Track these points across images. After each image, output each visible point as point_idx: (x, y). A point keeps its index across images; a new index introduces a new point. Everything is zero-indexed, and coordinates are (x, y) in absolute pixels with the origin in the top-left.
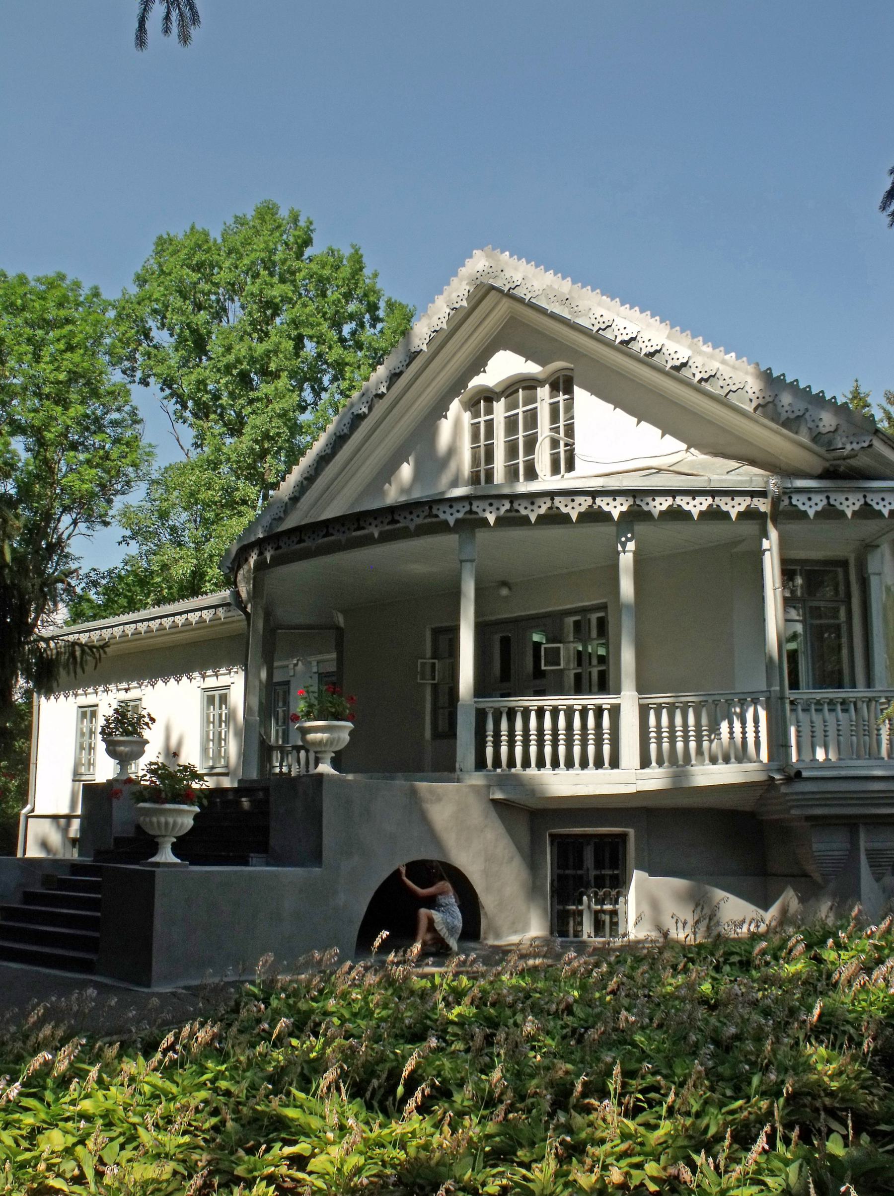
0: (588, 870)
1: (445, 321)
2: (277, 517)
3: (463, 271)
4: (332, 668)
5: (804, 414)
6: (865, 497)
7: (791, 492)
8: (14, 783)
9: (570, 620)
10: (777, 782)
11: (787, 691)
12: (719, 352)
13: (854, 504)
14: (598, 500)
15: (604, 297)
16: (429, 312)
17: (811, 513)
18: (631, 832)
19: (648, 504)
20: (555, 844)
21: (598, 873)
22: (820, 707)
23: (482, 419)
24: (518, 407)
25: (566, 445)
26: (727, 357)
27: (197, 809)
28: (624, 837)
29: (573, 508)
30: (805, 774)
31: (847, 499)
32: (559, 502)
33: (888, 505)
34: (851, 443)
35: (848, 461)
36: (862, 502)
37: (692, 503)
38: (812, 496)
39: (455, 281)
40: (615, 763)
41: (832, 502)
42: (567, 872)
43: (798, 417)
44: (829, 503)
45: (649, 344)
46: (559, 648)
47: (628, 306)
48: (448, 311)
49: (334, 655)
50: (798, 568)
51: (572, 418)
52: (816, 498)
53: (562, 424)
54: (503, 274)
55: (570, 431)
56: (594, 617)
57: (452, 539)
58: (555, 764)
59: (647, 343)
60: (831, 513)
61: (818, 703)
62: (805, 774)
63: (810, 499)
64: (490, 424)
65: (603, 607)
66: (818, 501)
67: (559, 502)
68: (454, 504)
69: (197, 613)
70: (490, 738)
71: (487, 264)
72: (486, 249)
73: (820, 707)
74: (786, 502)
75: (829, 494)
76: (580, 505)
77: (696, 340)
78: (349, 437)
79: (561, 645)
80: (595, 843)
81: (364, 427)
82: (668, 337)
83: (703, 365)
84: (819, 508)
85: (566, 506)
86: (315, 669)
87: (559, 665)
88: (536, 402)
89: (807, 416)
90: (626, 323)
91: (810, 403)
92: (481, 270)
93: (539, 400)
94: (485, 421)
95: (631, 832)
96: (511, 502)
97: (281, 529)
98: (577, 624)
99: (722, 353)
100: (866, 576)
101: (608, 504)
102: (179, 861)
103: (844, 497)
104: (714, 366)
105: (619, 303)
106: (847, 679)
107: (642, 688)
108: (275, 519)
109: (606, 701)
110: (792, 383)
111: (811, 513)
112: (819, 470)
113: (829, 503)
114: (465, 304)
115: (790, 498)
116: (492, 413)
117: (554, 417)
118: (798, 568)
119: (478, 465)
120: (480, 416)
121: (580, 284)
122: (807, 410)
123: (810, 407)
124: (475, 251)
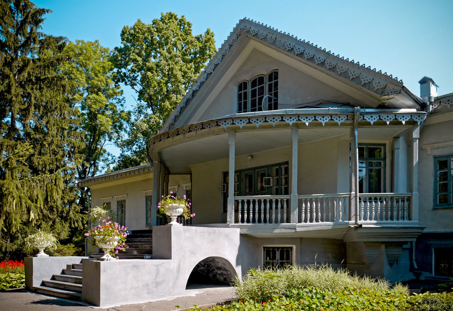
0: (278, 260)
4: (189, 189)
6: (380, 116)
7: (364, 114)
11: (358, 194)
13: (374, 119)
17: (372, 123)
18: (294, 247)
20: (265, 251)
21: (281, 261)
23: (243, 92)
25: (275, 100)
28: (291, 248)
30: (363, 226)
31: (388, 117)
35: (389, 100)
36: (394, 118)
38: (373, 115)
41: (381, 118)
42: (284, 261)
43: (369, 82)
44: (380, 119)
45: (308, 55)
46: (270, 179)
50: (365, 147)
51: (277, 89)
52: (374, 116)
53: (273, 92)
55: (276, 95)
56: (283, 167)
59: (308, 55)
60: (381, 123)
61: (370, 199)
62: (363, 226)
64: (245, 94)
65: (287, 163)
66: (261, 120)
70: (246, 211)
74: (362, 118)
75: (380, 115)
76: (406, 118)
79: (271, 178)
84: (376, 120)
87: (270, 185)
88: (263, 84)
90: (300, 47)
101: (337, 119)
106: (367, 149)
107: (299, 193)
110: (368, 68)
111: (372, 123)
112: (377, 106)
113: (380, 119)
115: (364, 116)
116: (246, 89)
117: (270, 90)
118: (365, 147)
120: (242, 91)
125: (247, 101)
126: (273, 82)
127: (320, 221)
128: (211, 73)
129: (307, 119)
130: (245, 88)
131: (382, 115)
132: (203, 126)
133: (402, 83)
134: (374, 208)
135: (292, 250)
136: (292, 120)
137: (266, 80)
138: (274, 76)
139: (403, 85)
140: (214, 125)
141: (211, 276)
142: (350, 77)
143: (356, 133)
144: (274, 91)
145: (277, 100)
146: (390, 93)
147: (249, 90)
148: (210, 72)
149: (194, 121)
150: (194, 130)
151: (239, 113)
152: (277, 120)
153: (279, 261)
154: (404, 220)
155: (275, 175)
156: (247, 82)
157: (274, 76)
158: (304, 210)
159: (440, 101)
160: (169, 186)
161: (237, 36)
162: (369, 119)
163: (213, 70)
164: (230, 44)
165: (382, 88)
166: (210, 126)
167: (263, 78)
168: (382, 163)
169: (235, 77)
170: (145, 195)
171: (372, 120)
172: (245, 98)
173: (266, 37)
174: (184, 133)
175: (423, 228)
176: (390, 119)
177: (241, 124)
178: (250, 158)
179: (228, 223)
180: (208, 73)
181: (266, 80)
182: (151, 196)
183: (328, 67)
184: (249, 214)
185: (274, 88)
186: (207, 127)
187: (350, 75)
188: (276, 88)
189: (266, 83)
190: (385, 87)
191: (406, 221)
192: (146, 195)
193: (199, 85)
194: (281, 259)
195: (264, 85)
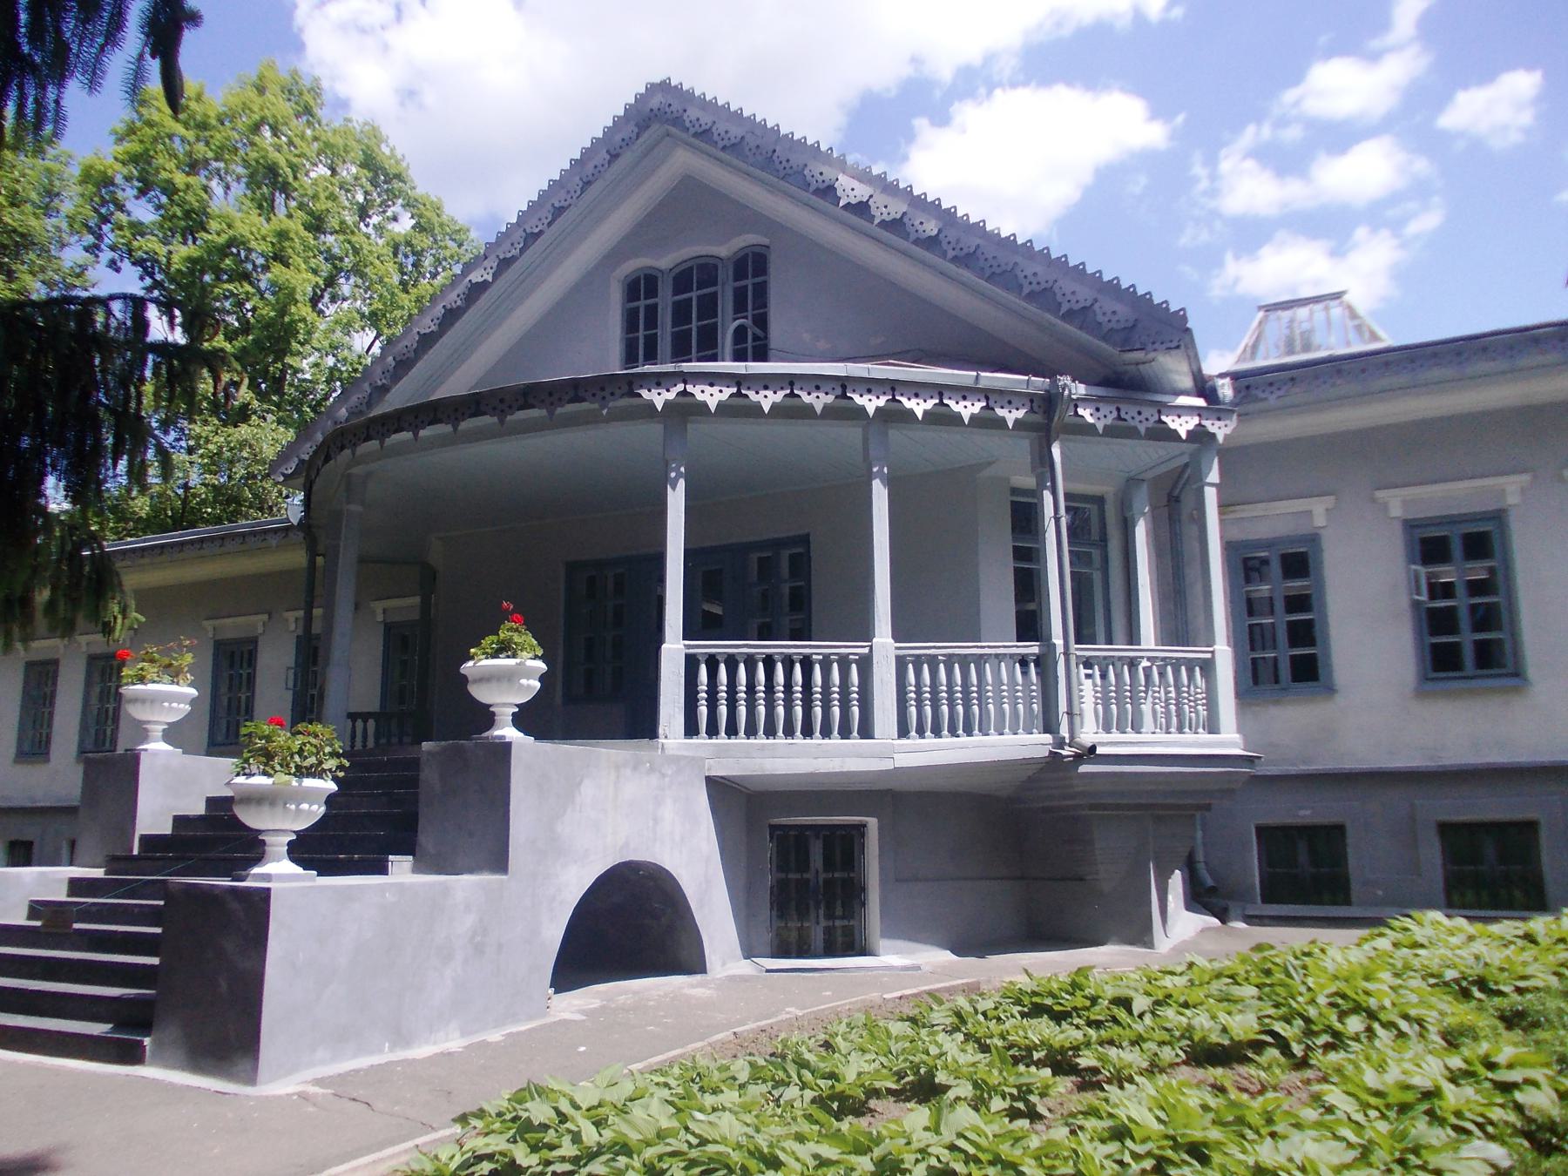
2: (355, 410)
5: (1092, 305)
8: (47, 711)
9: (754, 556)
13: (1147, 419)
18: (872, 823)
22: (1090, 672)
23: (642, 304)
25: (756, 338)
27: (332, 786)
28: (861, 828)
30: (1099, 751)
33: (1184, 424)
40: (866, 732)
41: (1123, 415)
43: (1084, 308)
51: (765, 306)
57: (655, 430)
58: (789, 732)
62: (1099, 751)
64: (652, 311)
66: (1107, 413)
73: (1090, 672)
78: (465, 312)
80: (825, 836)
81: (484, 300)
83: (958, 241)
85: (809, 394)
89: (1096, 306)
91: (1099, 291)
95: (872, 823)
97: (377, 411)
98: (793, 559)
100: (1128, 515)
108: (353, 413)
109: (855, 649)
113: (1119, 418)
117: (740, 307)
122: (1096, 300)
126: (749, 282)
127: (992, 731)
128: (541, 232)
130: (652, 291)
133: (1184, 319)
134: (990, 694)
135: (863, 835)
137: (726, 276)
138: (753, 264)
139: (1188, 325)
140: (618, 392)
142: (1021, 287)
143: (1056, 451)
144: (753, 310)
145: (766, 338)
146: (1150, 347)
147: (666, 300)
148: (536, 230)
149: (457, 385)
150: (494, 409)
151: (626, 369)
153: (822, 876)
157: (753, 264)
158: (743, 695)
160: (315, 604)
161: (636, 130)
164: (613, 152)
165: (1125, 328)
166: (603, 394)
167: (715, 267)
168: (1096, 554)
169: (614, 256)
170: (210, 635)
172: (652, 321)
173: (740, 142)
174: (502, 411)
176: (1147, 419)
179: (661, 740)
180: (528, 231)
181: (726, 276)
183: (951, 254)
184: (716, 707)
185: (754, 303)
186: (594, 395)
187: (1025, 283)
189: (723, 284)
190: (1134, 326)
191: (1203, 736)
192: (217, 638)
194: (826, 870)
195: (719, 288)
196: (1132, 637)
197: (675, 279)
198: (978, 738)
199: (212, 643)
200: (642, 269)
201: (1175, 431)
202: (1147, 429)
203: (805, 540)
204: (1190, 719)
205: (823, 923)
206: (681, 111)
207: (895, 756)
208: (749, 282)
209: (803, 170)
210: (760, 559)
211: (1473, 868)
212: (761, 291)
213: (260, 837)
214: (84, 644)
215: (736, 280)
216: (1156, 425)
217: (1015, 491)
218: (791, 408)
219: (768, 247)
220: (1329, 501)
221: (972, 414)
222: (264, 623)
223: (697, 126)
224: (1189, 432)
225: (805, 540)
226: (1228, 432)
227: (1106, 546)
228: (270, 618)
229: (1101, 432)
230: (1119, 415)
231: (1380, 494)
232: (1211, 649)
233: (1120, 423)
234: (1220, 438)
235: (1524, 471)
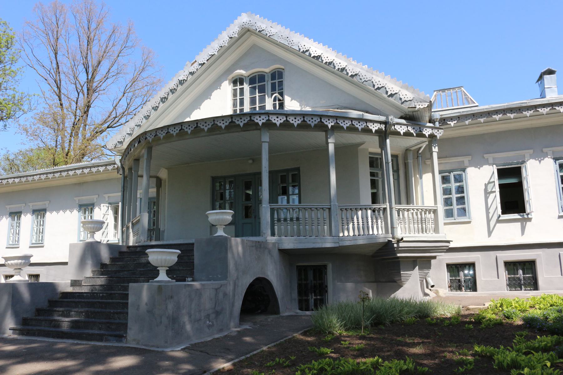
1: (226, 42)
3: (236, 22)
6: (420, 128)
10: (393, 242)
12: (360, 65)
13: (347, 124)
14: (271, 116)
15: (306, 38)
16: (218, 38)
19: (326, 122)
24: (256, 83)
26: (364, 67)
29: (312, 122)
30: (404, 239)
32: (355, 123)
33: (346, 124)
34: (419, 105)
36: (302, 119)
37: (373, 126)
39: (232, 26)
47: (317, 42)
48: (228, 38)
49: (120, 194)
51: (282, 89)
54: (256, 24)
62: (404, 239)
63: (344, 121)
66: (299, 119)
67: (355, 123)
68: (261, 116)
69: (6, 180)
71: (248, 19)
72: (247, 13)
77: (349, 59)
82: (336, 57)
83: (353, 69)
86: (31, 208)
88: (265, 81)
92: (245, 22)
93: (266, 80)
94: (240, 89)
96: (286, 117)
99: (362, 65)
101: (292, 120)
102: (170, 280)
103: (328, 119)
104: (357, 70)
105: (313, 41)
114: (236, 36)
119: (236, 107)
120: (237, 86)
121: (294, 32)
123: (400, 89)
124: (242, 14)
125: (243, 98)
128: (204, 63)
129: (241, 120)
131: (409, 127)
132: (232, 120)
135: (326, 269)
136: (361, 125)
137: (268, 78)
141: (277, 358)
145: (283, 100)
148: (202, 63)
152: (315, 121)
154: (419, 233)
155: (291, 182)
156: (244, 78)
159: (277, 116)
162: (326, 122)
163: (207, 60)
167: (264, 76)
171: (223, 124)
175: (448, 242)
177: (278, 121)
178: (250, 161)
181: (268, 78)
182: (534, 285)
188: (281, 88)
189: (267, 81)
193: (187, 75)
195: (266, 83)
196: (400, 202)
197: (250, 79)
198: (425, 234)
199: (78, 205)
200: (238, 75)
201: (425, 134)
202: (429, 135)
203: (298, 169)
204: (153, 234)
205: (314, 297)
206: (254, 23)
207: (339, 242)
208: (277, 81)
209: (298, 44)
210: (281, 176)
211: (513, 276)
212: (281, 84)
213: (158, 269)
214: (31, 206)
215: (272, 80)
216: (419, 132)
217: (370, 153)
218: (420, 134)
219: (283, 69)
220: (470, 158)
221: (376, 130)
222: (97, 199)
223: (260, 28)
224: (376, 131)
225: (298, 169)
226: (441, 135)
227: (399, 172)
228: (98, 197)
229: (402, 134)
230: (304, 119)
231: (485, 156)
232: (436, 206)
233: (353, 126)
234: (438, 137)
235: (531, 149)
